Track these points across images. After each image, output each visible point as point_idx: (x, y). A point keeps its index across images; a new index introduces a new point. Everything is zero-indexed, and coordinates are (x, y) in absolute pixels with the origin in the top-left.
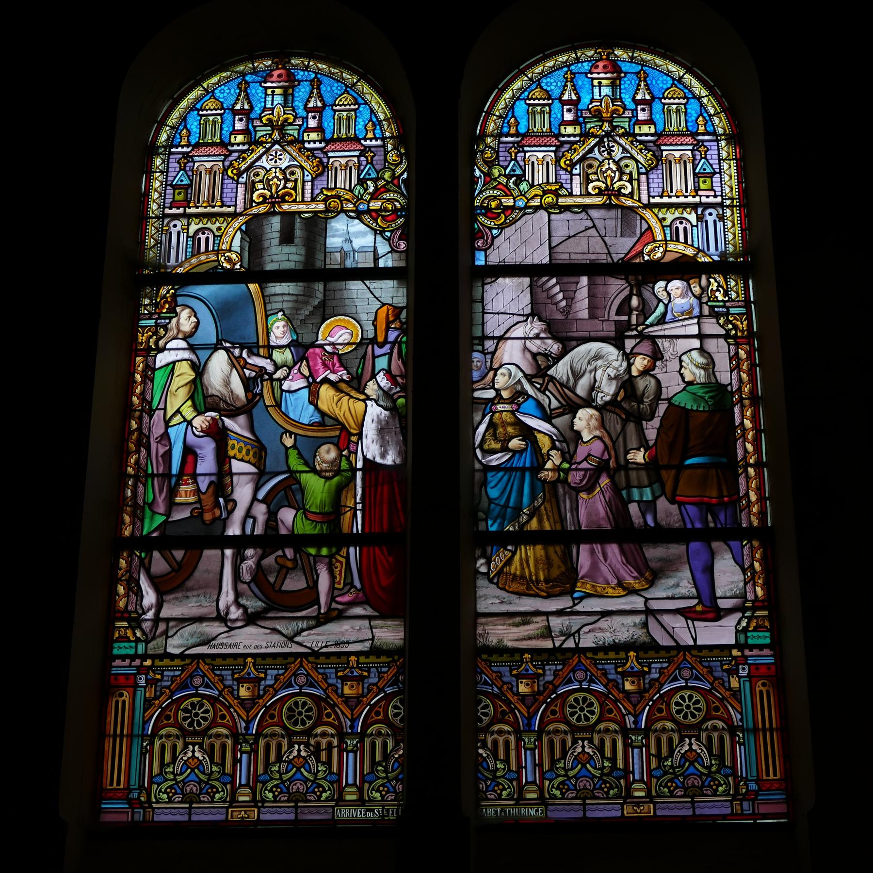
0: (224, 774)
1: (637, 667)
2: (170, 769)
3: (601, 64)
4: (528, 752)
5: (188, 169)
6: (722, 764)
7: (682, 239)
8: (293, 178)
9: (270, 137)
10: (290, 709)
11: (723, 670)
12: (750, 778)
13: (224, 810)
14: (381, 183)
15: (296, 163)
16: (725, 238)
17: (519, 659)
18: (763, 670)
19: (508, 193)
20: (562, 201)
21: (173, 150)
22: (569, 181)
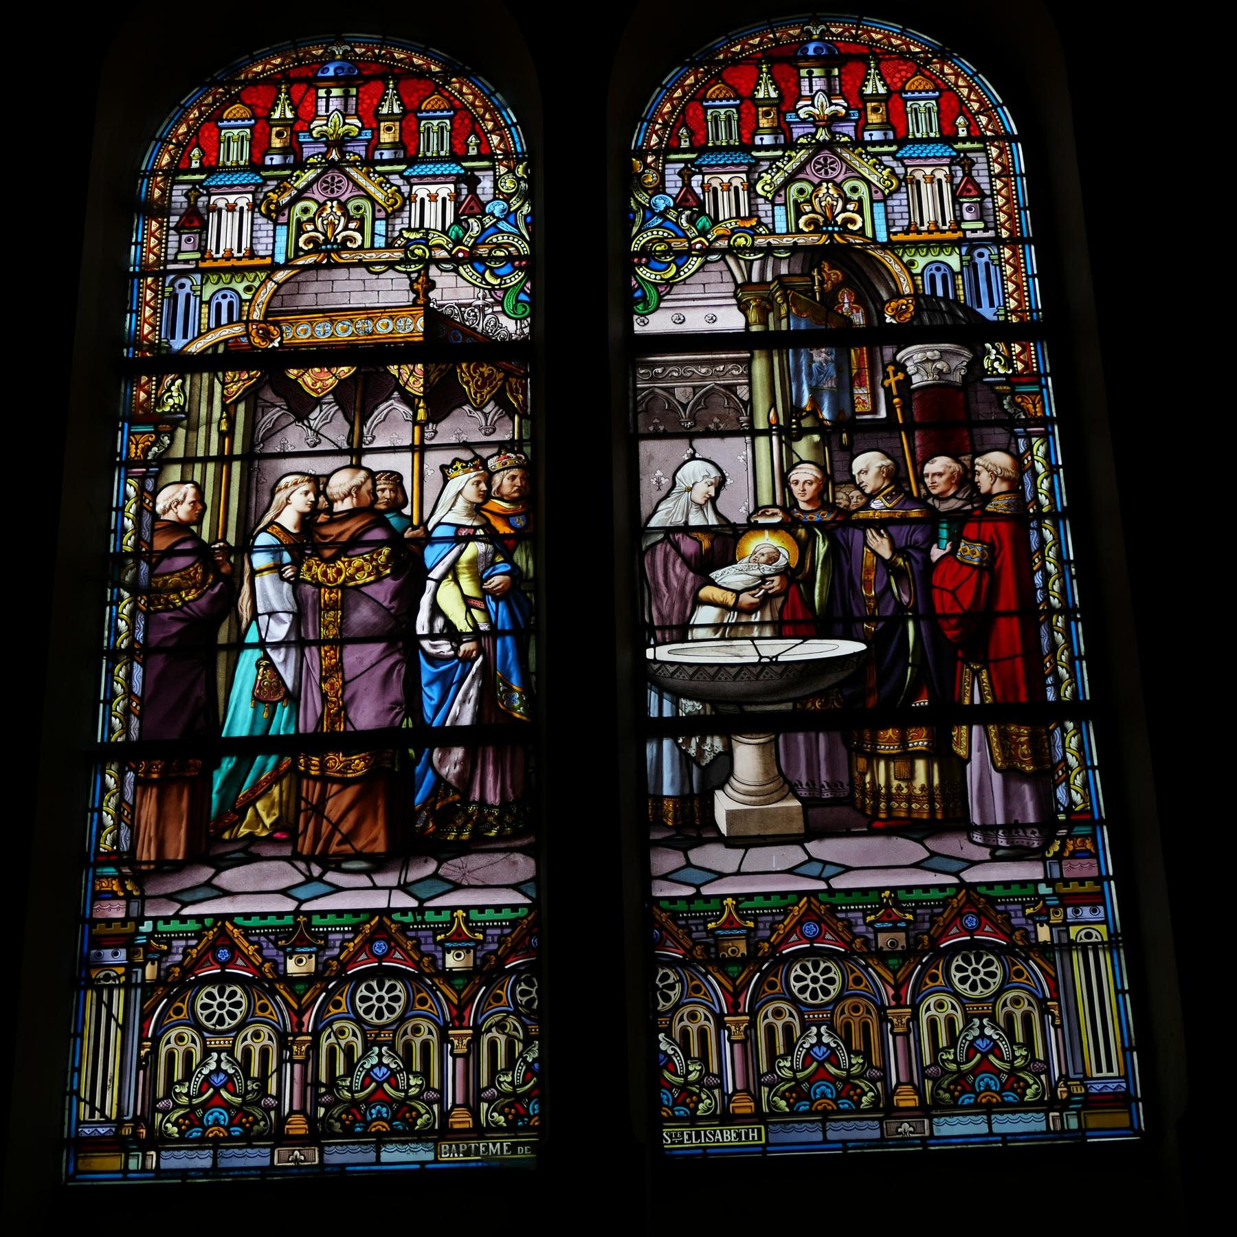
4: (899, 1039)
8: (855, 197)
12: (1072, 1075)
13: (876, 1123)
14: (488, 221)
16: (1003, 289)
22: (770, 213)
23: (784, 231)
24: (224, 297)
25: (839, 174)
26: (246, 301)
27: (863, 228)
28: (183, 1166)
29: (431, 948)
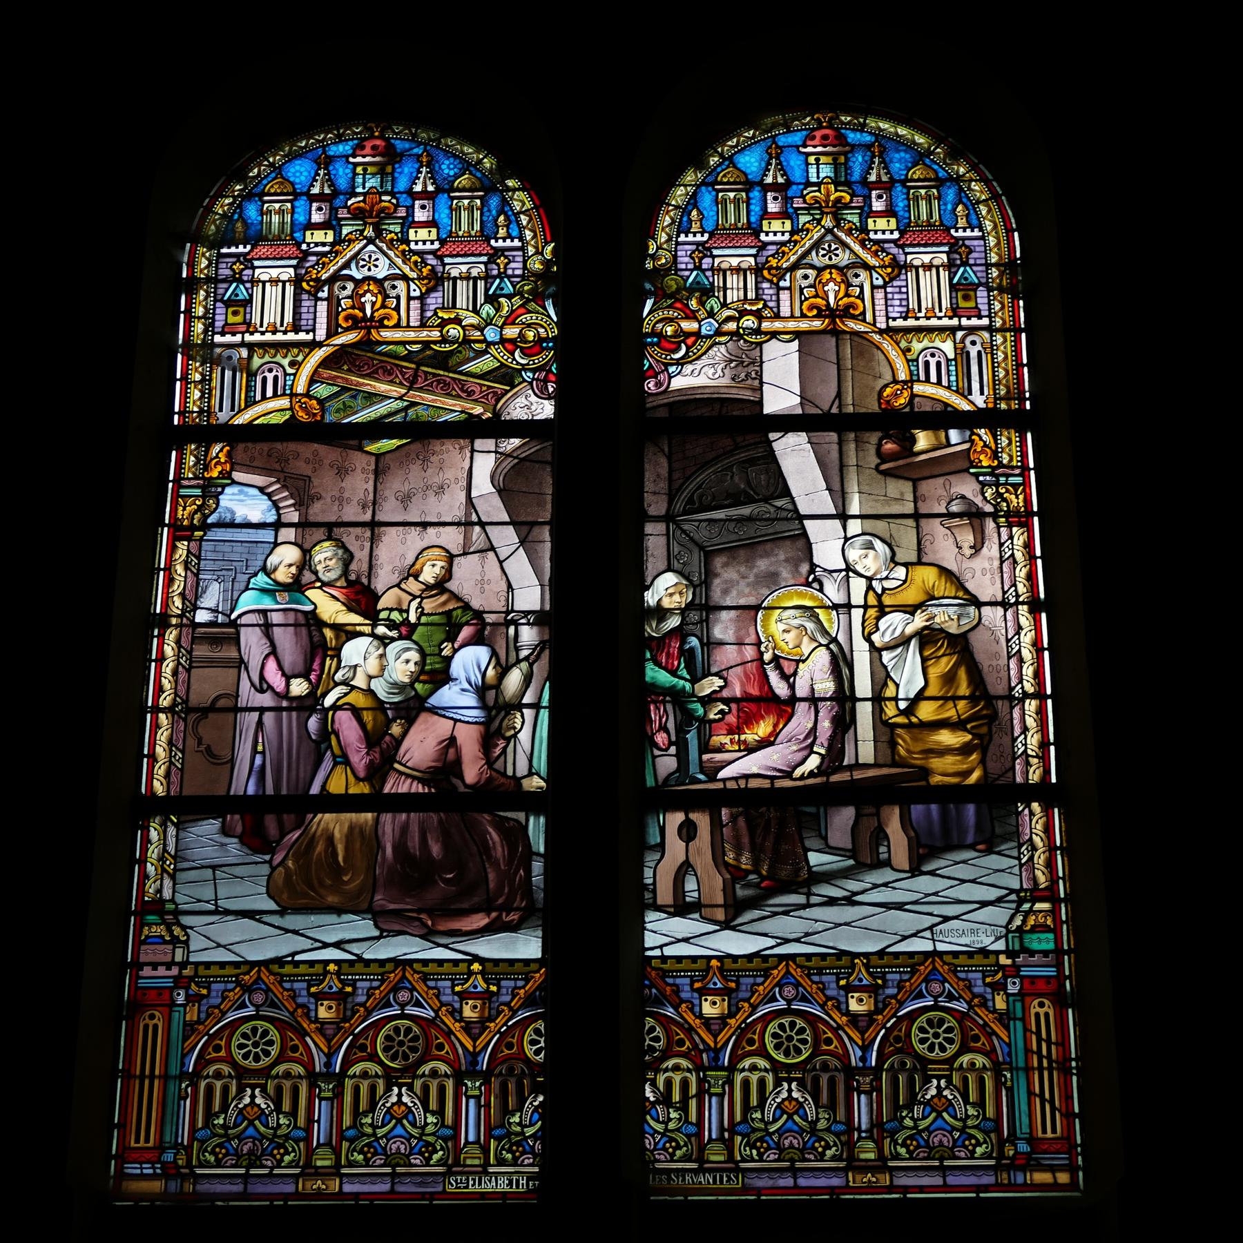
0: (985, 1118)
1: (482, 985)
2: (516, 1119)
3: (818, 134)
4: (714, 1099)
5: (704, 266)
7: (933, 378)
10: (388, 1038)
11: (454, 993)
15: (398, 271)
16: (994, 376)
18: (1041, 986)
19: (691, 316)
20: (766, 325)
23: (788, 314)
24: (270, 370)
26: (290, 375)
27: (864, 313)
28: (355, 1191)
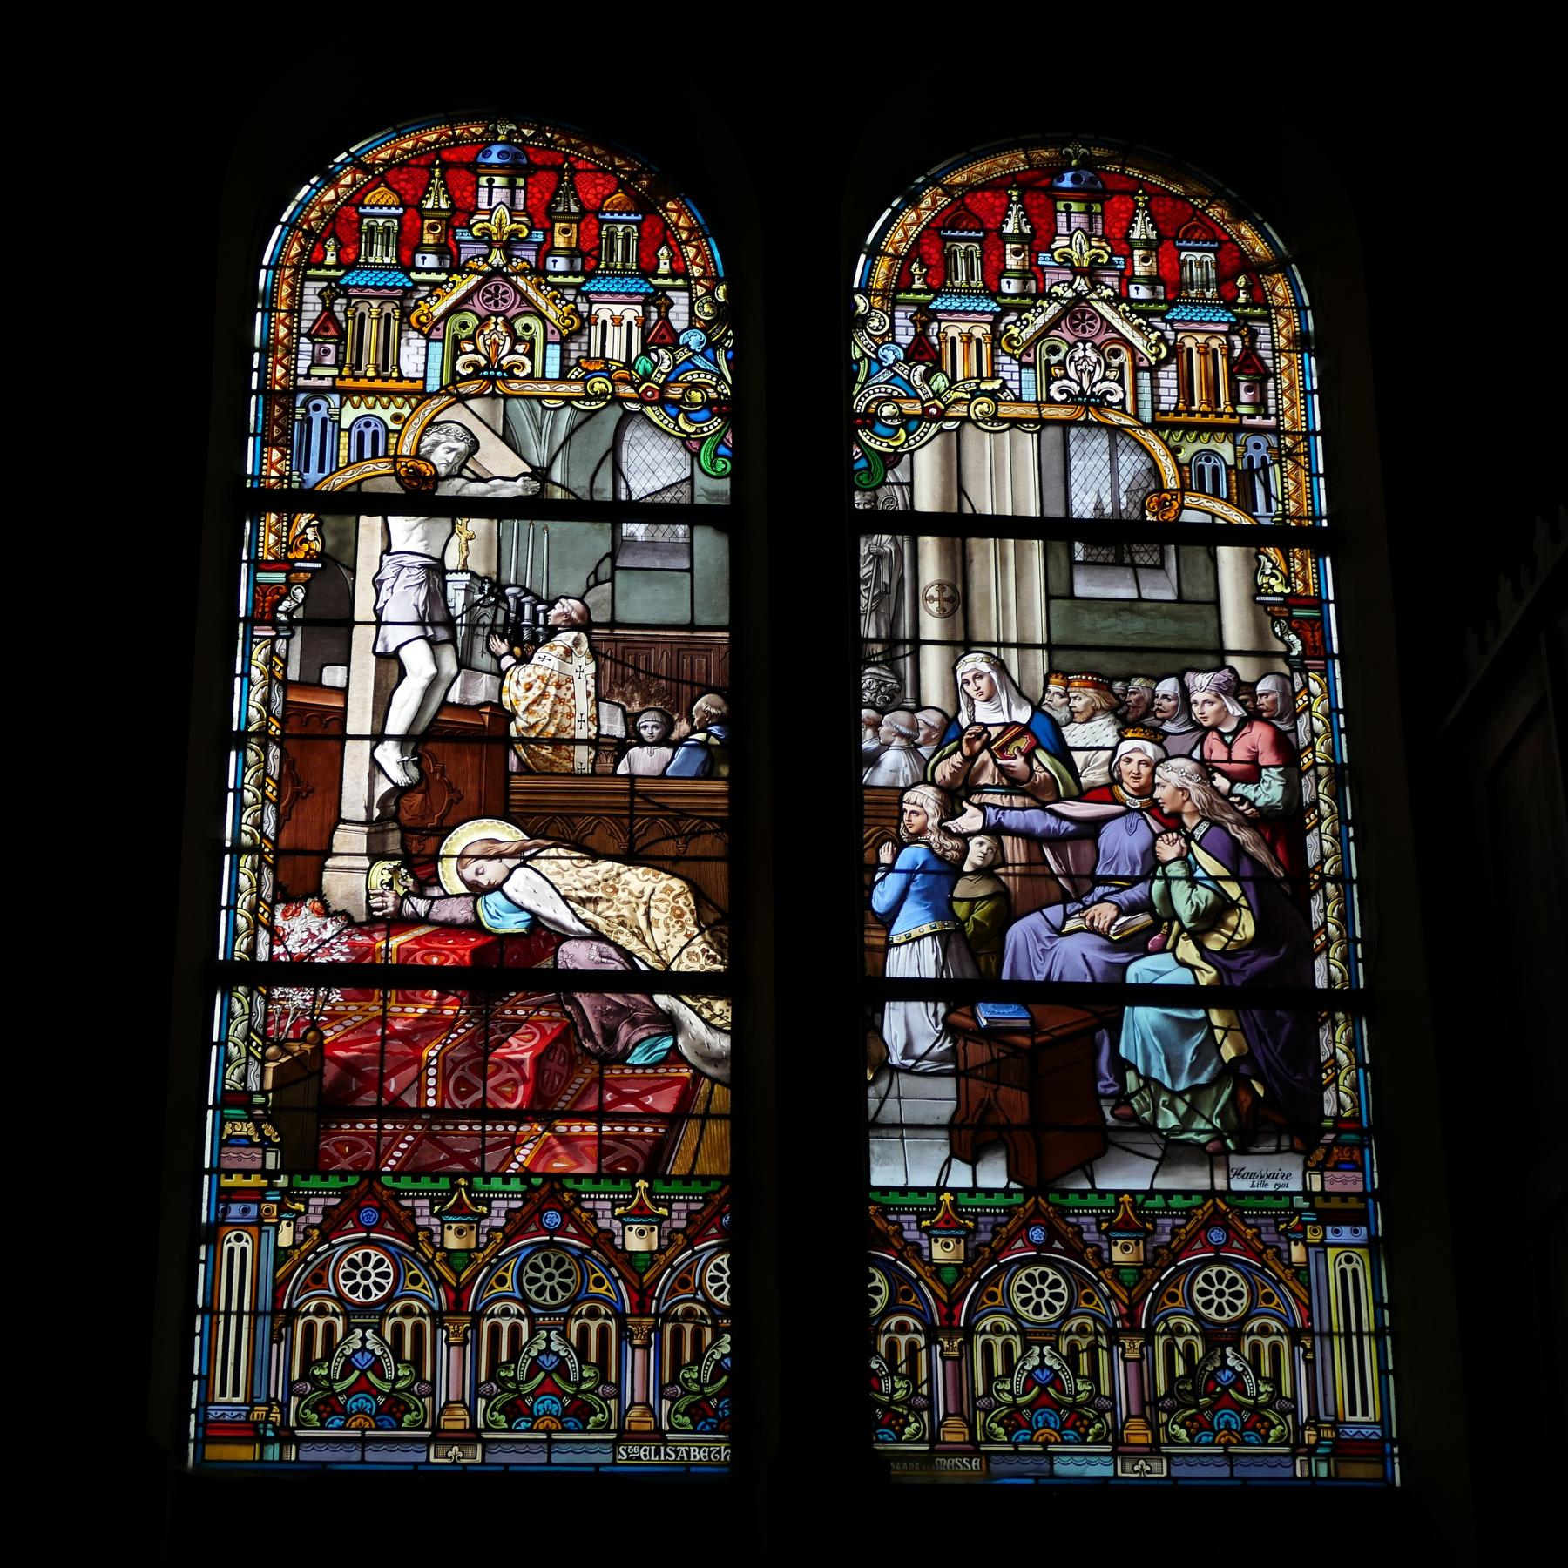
6: (603, 1379)
9: (485, 261)
14: (682, 356)
17: (629, 1189)
20: (1004, 411)
21: (311, 272)
22: (1016, 376)
25: (512, 305)
26: (394, 431)
27: (1122, 402)
29: (1273, 1238)
